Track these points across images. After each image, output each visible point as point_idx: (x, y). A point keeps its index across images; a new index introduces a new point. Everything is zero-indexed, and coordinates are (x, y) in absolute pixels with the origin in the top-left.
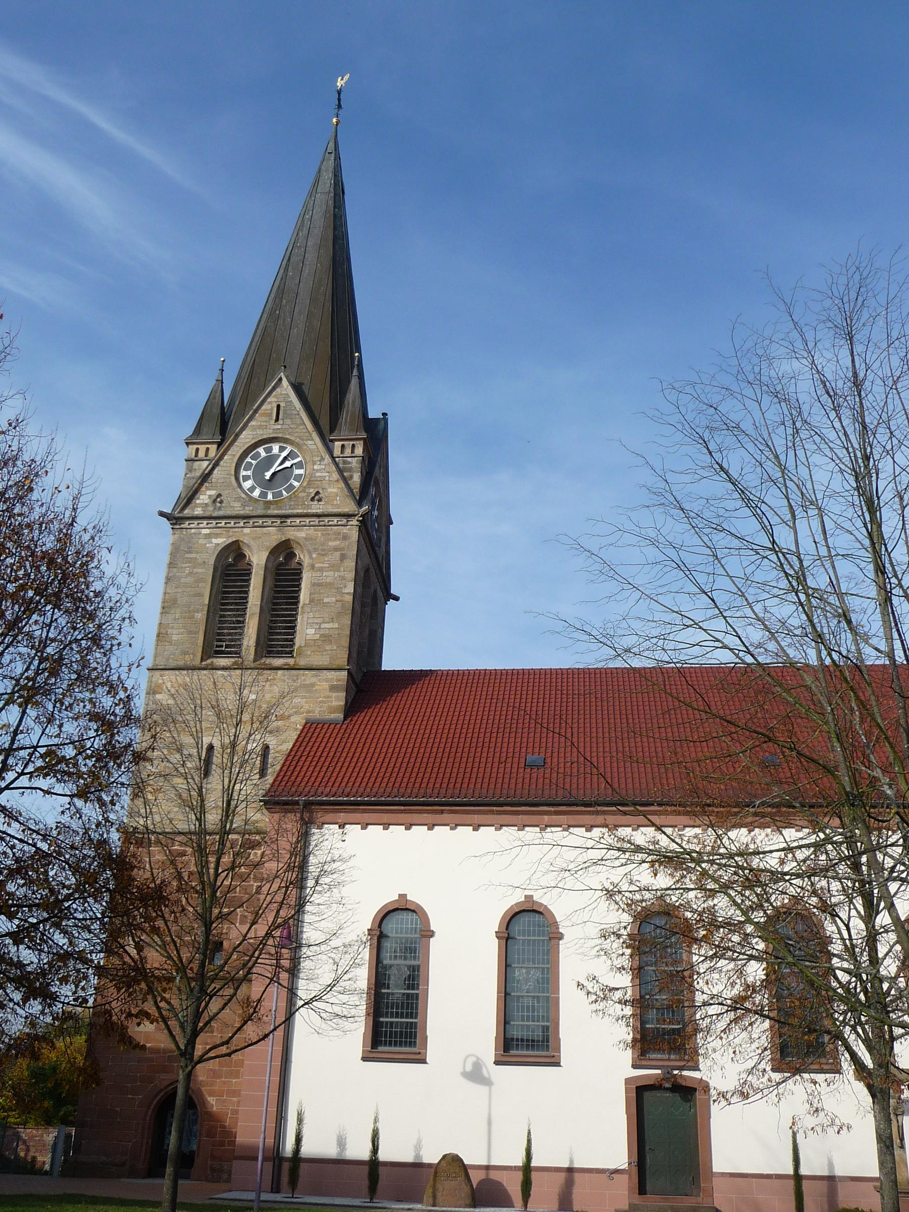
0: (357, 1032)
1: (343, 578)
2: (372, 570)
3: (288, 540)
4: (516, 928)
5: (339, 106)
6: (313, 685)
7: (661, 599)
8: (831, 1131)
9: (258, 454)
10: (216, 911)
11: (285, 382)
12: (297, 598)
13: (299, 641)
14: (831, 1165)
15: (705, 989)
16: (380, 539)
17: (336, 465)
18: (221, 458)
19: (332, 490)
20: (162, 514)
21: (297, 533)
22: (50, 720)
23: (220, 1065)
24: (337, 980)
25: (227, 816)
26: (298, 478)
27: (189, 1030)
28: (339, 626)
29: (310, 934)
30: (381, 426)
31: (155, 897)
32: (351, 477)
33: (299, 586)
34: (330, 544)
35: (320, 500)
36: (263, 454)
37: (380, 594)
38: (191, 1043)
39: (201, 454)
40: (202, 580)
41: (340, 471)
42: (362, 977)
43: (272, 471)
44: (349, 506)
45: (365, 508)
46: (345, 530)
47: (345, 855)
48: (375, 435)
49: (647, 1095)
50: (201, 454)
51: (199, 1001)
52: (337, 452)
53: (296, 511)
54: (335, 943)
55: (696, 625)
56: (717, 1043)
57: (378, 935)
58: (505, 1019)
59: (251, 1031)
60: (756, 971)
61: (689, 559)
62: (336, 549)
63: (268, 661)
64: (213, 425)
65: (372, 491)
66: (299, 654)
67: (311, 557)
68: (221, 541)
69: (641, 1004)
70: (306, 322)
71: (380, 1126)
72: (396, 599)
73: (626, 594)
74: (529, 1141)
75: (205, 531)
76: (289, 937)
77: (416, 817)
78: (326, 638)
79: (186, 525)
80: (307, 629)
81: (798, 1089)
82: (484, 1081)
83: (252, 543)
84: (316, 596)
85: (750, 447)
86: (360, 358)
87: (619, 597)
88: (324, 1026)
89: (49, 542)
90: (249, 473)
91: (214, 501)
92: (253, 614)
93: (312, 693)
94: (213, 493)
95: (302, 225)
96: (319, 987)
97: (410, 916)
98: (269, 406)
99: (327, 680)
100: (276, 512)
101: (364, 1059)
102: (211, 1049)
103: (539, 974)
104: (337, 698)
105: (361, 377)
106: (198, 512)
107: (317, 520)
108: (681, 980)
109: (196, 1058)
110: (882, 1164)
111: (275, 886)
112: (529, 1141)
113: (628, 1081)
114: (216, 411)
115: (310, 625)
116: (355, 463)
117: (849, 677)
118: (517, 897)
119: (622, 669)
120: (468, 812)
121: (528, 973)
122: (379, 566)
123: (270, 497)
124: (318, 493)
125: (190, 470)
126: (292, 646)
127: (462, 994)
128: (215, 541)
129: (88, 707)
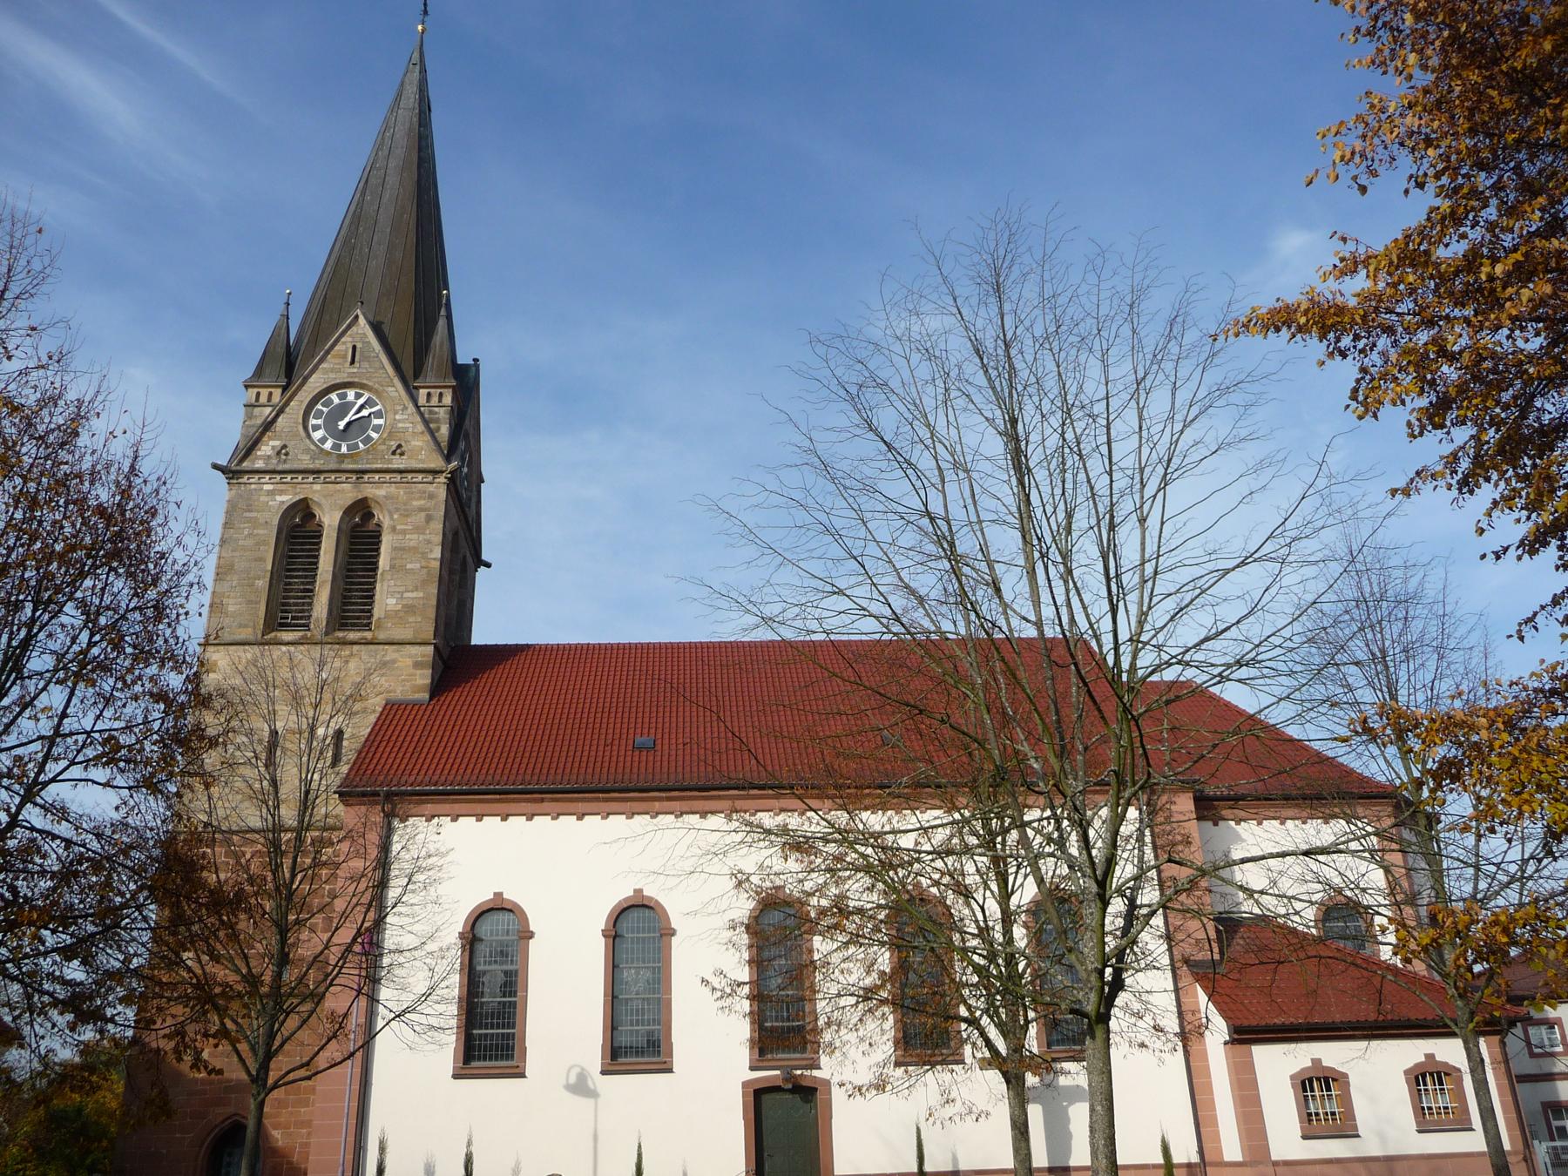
0: (449, 1043)
1: (429, 542)
2: (461, 533)
3: (365, 499)
4: (624, 925)
5: (426, 12)
6: (394, 661)
7: (801, 564)
8: (970, 1119)
9: (331, 401)
10: (292, 918)
11: (362, 320)
12: (376, 563)
13: (377, 612)
14: (955, 1160)
15: (841, 978)
16: (470, 499)
17: (422, 415)
18: (287, 404)
19: (417, 443)
20: (216, 467)
21: (376, 491)
22: (108, 700)
23: (287, 1093)
24: (432, 988)
25: (306, 808)
26: (377, 429)
27: (261, 1052)
28: (425, 596)
29: (391, 938)
30: (472, 373)
31: (225, 903)
32: (438, 429)
33: (378, 550)
34: (415, 503)
35: (402, 454)
36: (336, 401)
37: (469, 560)
38: (264, 1068)
39: (263, 399)
40: (265, 543)
41: (426, 422)
42: (453, 986)
43: (347, 420)
44: (437, 462)
45: (455, 464)
46: (431, 488)
47: (443, 849)
48: (465, 382)
49: (766, 1098)
50: (263, 399)
51: (273, 1018)
52: (422, 400)
53: (374, 466)
54: (431, 947)
55: (840, 592)
56: (852, 1037)
57: (471, 939)
58: (613, 1024)
59: (333, 1051)
60: (885, 960)
61: (838, 523)
62: (421, 509)
63: (341, 634)
64: (279, 366)
65: (462, 445)
66: (378, 627)
67: (392, 518)
68: (287, 499)
69: (758, 997)
70: (386, 251)
71: (474, 1149)
72: (488, 565)
73: (767, 559)
74: (640, 1156)
75: (266, 487)
76: (370, 943)
77: (513, 807)
78: (410, 609)
79: (245, 479)
80: (387, 599)
81: (933, 1081)
82: (592, 1094)
83: (323, 501)
84: (398, 563)
85: (898, 404)
86: (448, 296)
87: (760, 562)
88: (417, 1039)
89: (103, 494)
90: (319, 422)
91: (279, 453)
92: (323, 582)
93: (405, 673)
94: (277, 443)
95: (382, 144)
96: (413, 997)
97: (506, 916)
98: (344, 346)
99: (410, 656)
100: (351, 467)
101: (456, 1076)
102: (288, 1073)
103: (649, 974)
104: (422, 676)
105: (449, 317)
106: (260, 464)
107: (399, 476)
108: (802, 973)
109: (270, 1082)
110: (1016, 1151)
111: (362, 886)
112: (640, 1156)
113: (745, 1085)
114: (281, 350)
115: (392, 594)
116: (442, 413)
117: (996, 651)
118: (624, 892)
119: (768, 642)
120: (571, 800)
121: (637, 973)
122: (470, 530)
123: (344, 449)
124: (399, 446)
125: (249, 416)
126: (370, 617)
127: (564, 1000)
128: (279, 498)
129: (148, 686)
